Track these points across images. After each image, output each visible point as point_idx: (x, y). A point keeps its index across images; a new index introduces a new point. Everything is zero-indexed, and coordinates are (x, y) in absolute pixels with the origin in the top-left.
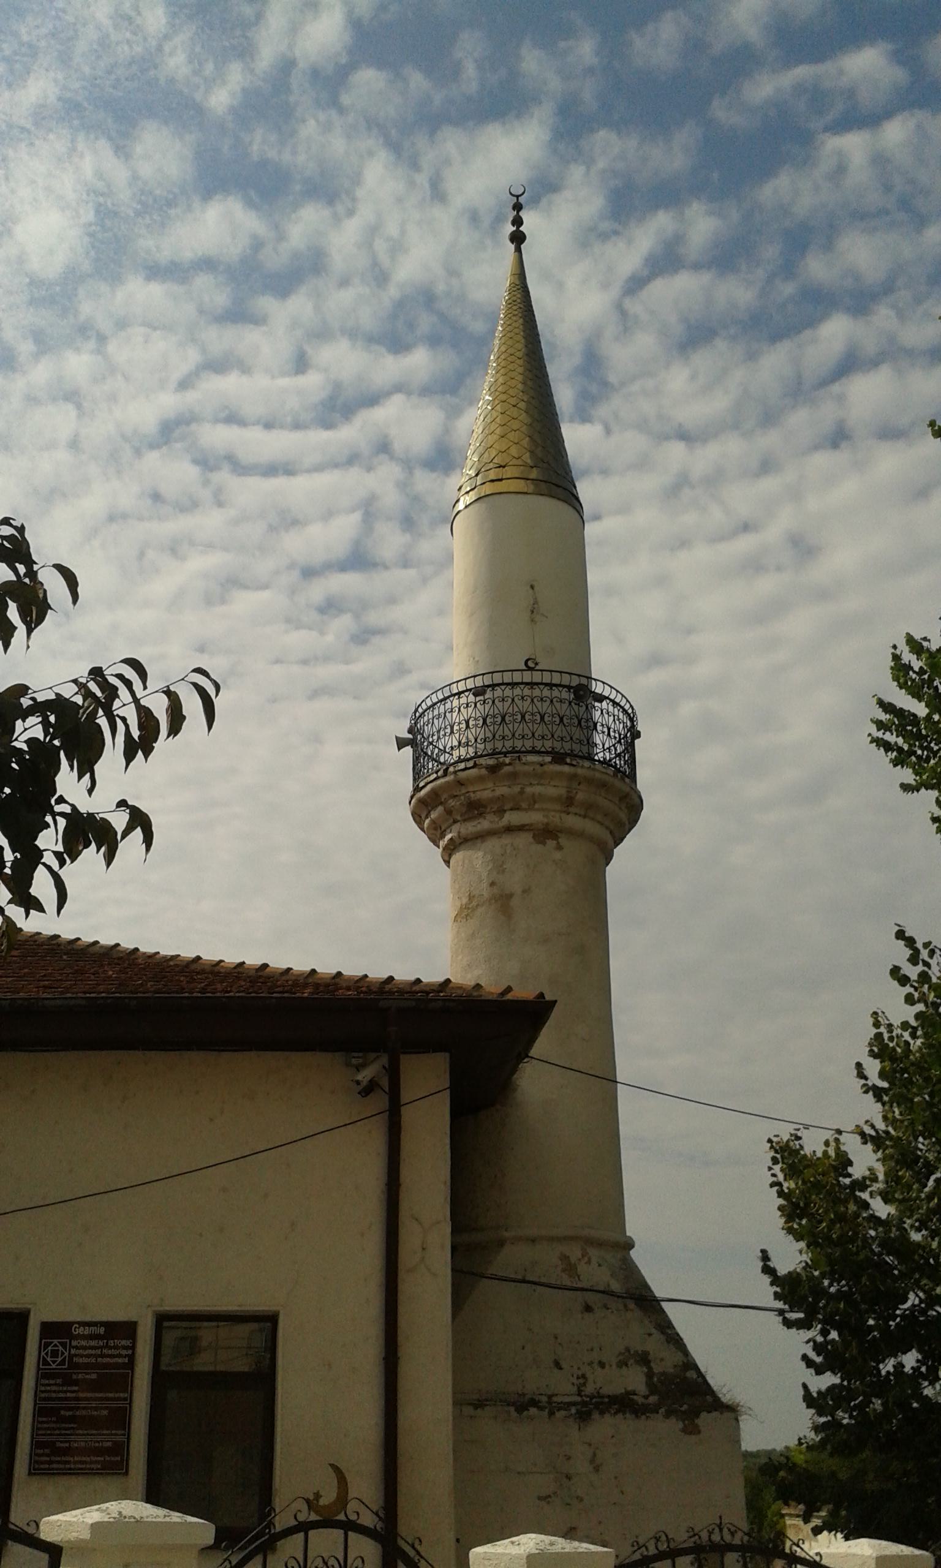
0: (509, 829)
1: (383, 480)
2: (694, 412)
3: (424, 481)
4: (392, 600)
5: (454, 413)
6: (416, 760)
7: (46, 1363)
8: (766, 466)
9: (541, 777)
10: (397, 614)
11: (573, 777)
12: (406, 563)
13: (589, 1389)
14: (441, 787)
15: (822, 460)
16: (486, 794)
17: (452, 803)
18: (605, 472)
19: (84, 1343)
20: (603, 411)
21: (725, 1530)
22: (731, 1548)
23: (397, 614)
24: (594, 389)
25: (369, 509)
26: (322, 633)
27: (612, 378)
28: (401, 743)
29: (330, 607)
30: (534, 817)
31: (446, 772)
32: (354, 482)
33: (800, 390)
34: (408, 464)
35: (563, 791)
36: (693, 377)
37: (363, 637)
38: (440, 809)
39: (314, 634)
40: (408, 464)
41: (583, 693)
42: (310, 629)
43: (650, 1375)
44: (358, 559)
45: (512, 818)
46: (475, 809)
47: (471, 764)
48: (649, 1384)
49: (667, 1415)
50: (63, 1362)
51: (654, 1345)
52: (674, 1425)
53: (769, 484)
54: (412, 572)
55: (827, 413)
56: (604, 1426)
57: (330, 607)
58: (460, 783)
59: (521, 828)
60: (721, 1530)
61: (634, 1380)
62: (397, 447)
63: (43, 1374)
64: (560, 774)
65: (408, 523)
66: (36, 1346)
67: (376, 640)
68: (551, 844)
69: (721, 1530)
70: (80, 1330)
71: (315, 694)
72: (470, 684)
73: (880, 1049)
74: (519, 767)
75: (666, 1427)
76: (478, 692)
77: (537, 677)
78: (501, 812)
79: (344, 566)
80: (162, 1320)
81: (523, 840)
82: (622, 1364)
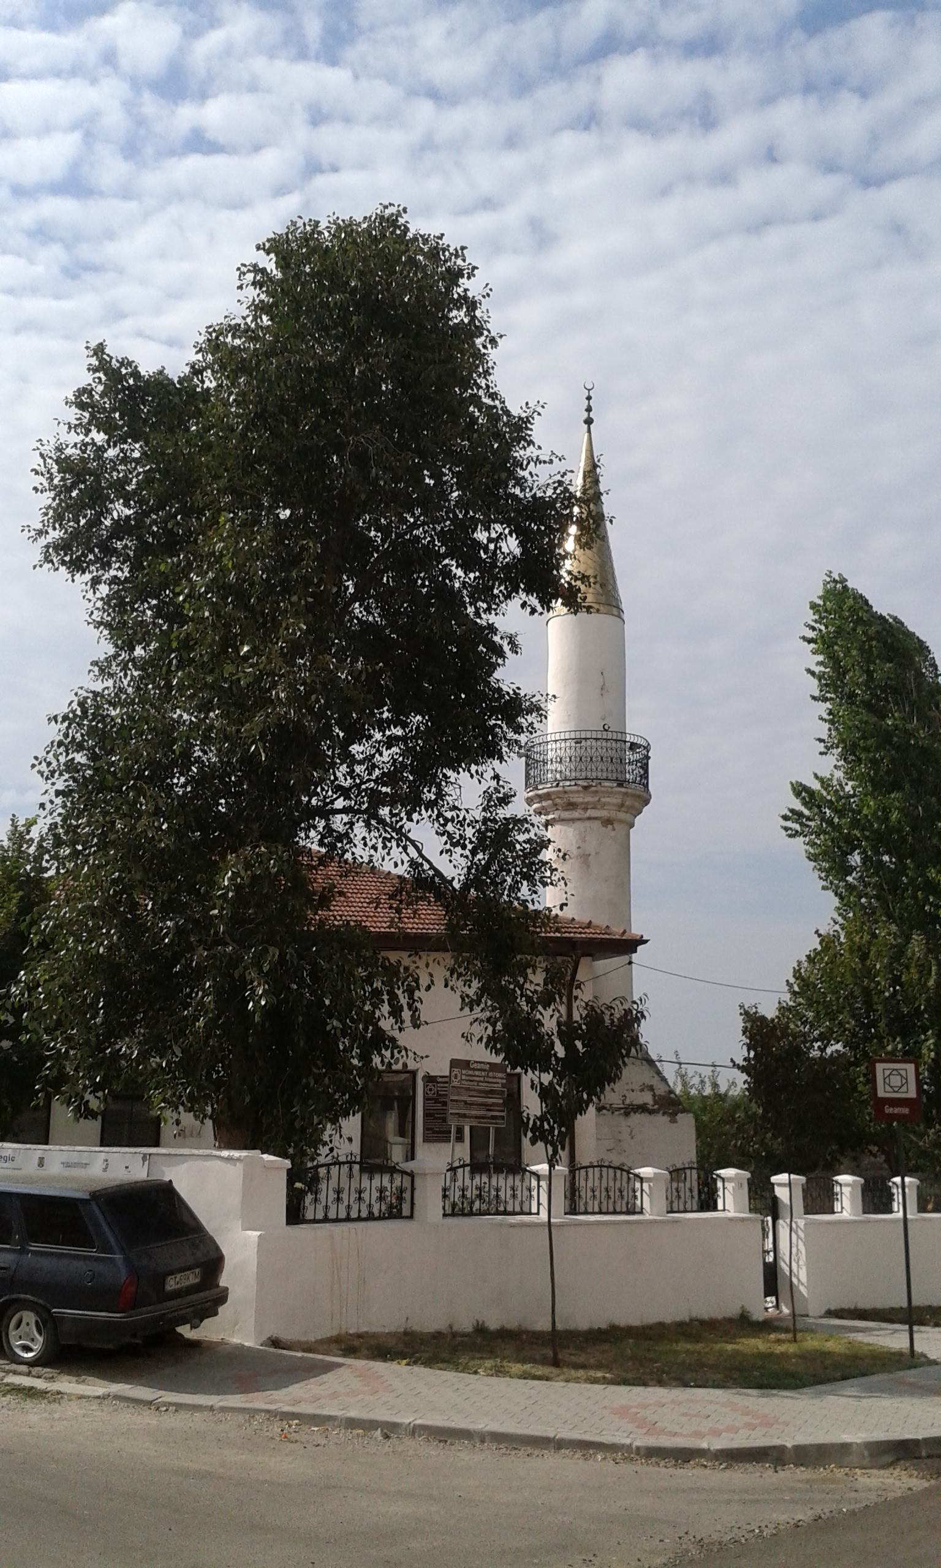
0: (589, 818)
1: (106, 96)
2: (447, 70)
4: (110, 235)
6: (527, 765)
8: (512, 141)
9: (610, 794)
10: (111, 250)
11: (626, 794)
12: (126, 193)
13: (627, 1102)
14: (553, 792)
15: (568, 141)
16: (581, 800)
17: (558, 801)
18: (348, 120)
20: (351, 54)
22: (355, 1163)
23: (111, 250)
24: (344, 26)
25: (88, 127)
26: (32, 261)
29: (42, 234)
31: (557, 785)
32: (80, 96)
33: (560, 66)
34: (136, 83)
35: (619, 801)
36: (450, 33)
37: (77, 271)
38: (550, 802)
39: (22, 262)
40: (136, 83)
43: (654, 1095)
44: (74, 184)
45: (591, 813)
46: (571, 806)
47: (573, 783)
48: (654, 1100)
49: (664, 1114)
51: (655, 1082)
52: (666, 1118)
53: (513, 161)
54: (133, 205)
55: (581, 92)
56: (636, 1118)
57: (42, 234)
58: (565, 792)
59: (595, 818)
61: (647, 1098)
62: (125, 63)
64: (620, 792)
65: (131, 150)
67: (88, 277)
68: (610, 827)
70: (440, 1080)
71: (21, 328)
72: (573, 735)
73: (797, 974)
74: (599, 788)
75: (662, 1119)
76: (578, 741)
78: (586, 809)
79: (58, 189)
81: (598, 823)
82: (642, 1090)
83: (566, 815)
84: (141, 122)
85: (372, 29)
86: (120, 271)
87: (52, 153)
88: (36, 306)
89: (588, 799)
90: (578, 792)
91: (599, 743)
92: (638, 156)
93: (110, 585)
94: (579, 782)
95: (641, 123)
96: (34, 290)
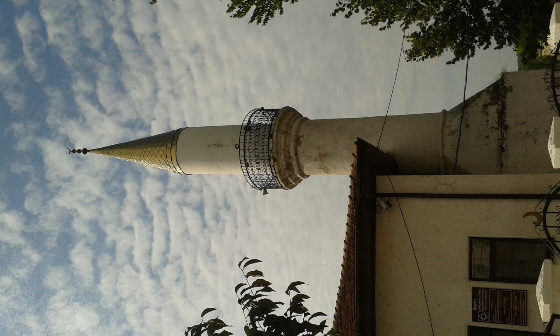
0: (296, 154)
1: (172, 199)
2: (147, 88)
3: (172, 184)
4: (214, 196)
5: (147, 174)
7: (487, 320)
8: (167, 62)
11: (278, 131)
12: (201, 191)
13: (496, 126)
15: (164, 42)
16: (284, 162)
17: (287, 175)
18: (169, 120)
19: (480, 306)
20: (147, 121)
21: (547, 77)
24: (139, 124)
25: (182, 204)
26: (226, 221)
27: (135, 117)
28: (265, 193)
29: (217, 218)
30: (292, 145)
31: (276, 177)
32: (172, 209)
33: (139, 51)
34: (166, 190)
36: (135, 89)
37: (227, 206)
38: (289, 179)
40: (166, 190)
41: (247, 128)
42: (224, 225)
43: (491, 104)
44: (200, 208)
45: (292, 153)
46: (289, 166)
47: (273, 168)
49: (505, 98)
50: (487, 314)
51: (480, 103)
52: (509, 95)
53: (173, 61)
54: (204, 189)
55: (147, 40)
56: (509, 120)
57: (217, 218)
58: (280, 172)
59: (296, 150)
60: (546, 79)
61: (493, 110)
62: (159, 194)
63: (491, 321)
65: (187, 190)
66: (481, 323)
67: (229, 202)
68: (301, 139)
69: (546, 79)
71: (248, 223)
72: (244, 168)
74: (274, 151)
75: (510, 99)
76: (247, 165)
77: (242, 144)
78: (290, 157)
79: (202, 213)
80: (471, 278)
81: (300, 149)
82: (487, 114)
83: (296, 168)
84: (178, 188)
85: (137, 114)
86: (226, 191)
87: (191, 216)
88: (240, 219)
89: (282, 157)
90: (278, 164)
91: (247, 151)
92: (165, 18)
93: (419, 50)
94: (272, 164)
95: (155, 18)
96: (235, 219)
